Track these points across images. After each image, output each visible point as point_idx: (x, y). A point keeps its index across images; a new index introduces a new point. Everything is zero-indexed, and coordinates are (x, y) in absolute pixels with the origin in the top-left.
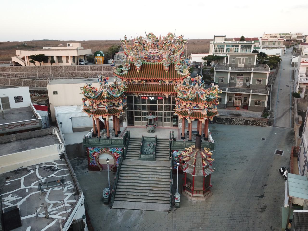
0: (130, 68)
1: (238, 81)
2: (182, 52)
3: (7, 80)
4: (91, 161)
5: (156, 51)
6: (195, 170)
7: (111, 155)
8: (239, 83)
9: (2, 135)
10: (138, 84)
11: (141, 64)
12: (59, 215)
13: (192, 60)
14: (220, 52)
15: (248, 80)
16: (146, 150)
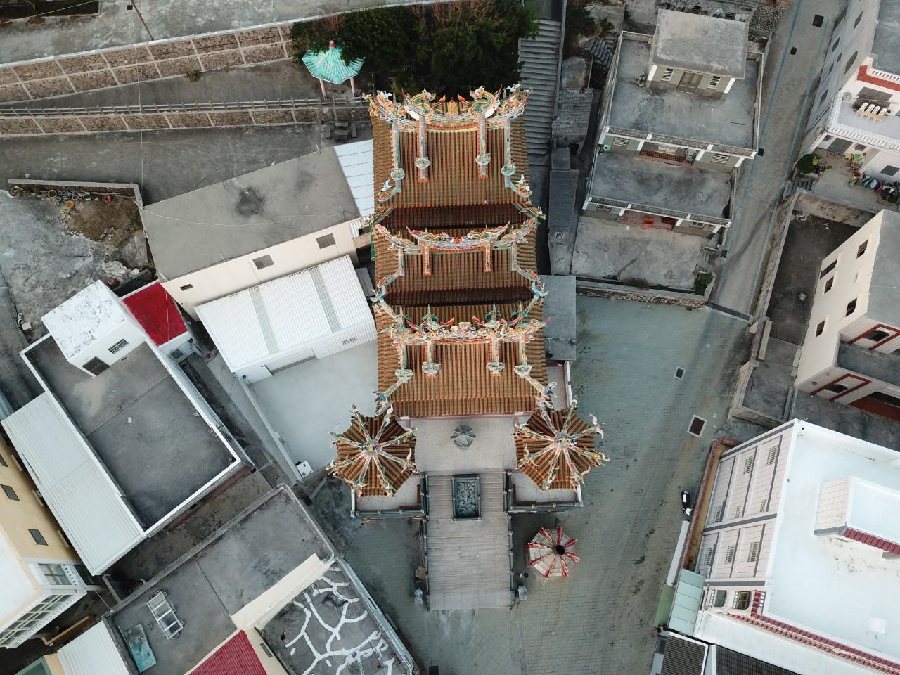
9: (17, 103)
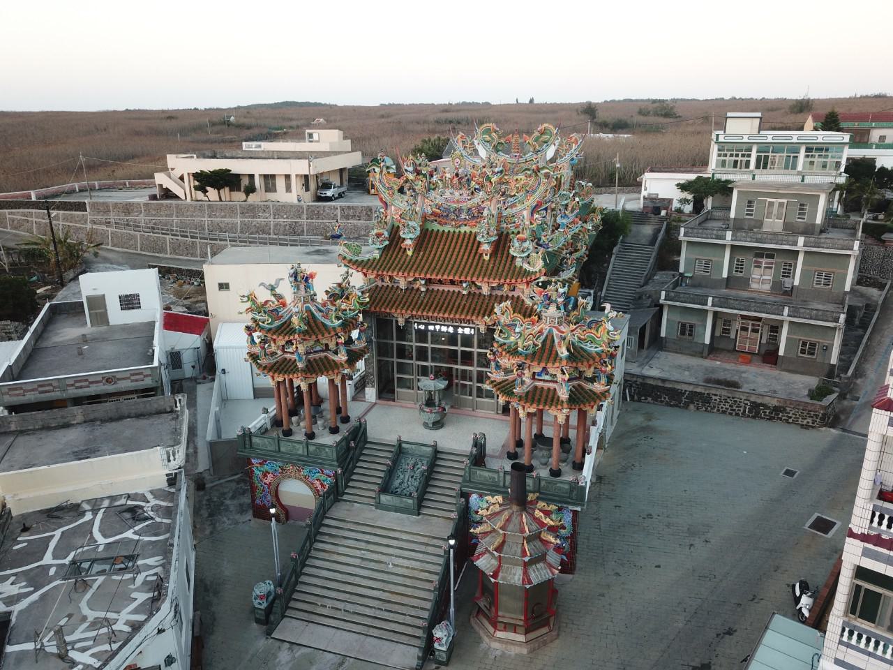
0: (387, 243)
1: (756, 274)
2: (538, 202)
3: (134, 237)
4: (258, 494)
5: (465, 196)
6: (507, 565)
7: (307, 484)
8: (761, 279)
10: (407, 289)
11: (418, 233)
12: (93, 655)
13: (645, 190)
14: (735, 166)
15: (788, 273)
16: (399, 481)
